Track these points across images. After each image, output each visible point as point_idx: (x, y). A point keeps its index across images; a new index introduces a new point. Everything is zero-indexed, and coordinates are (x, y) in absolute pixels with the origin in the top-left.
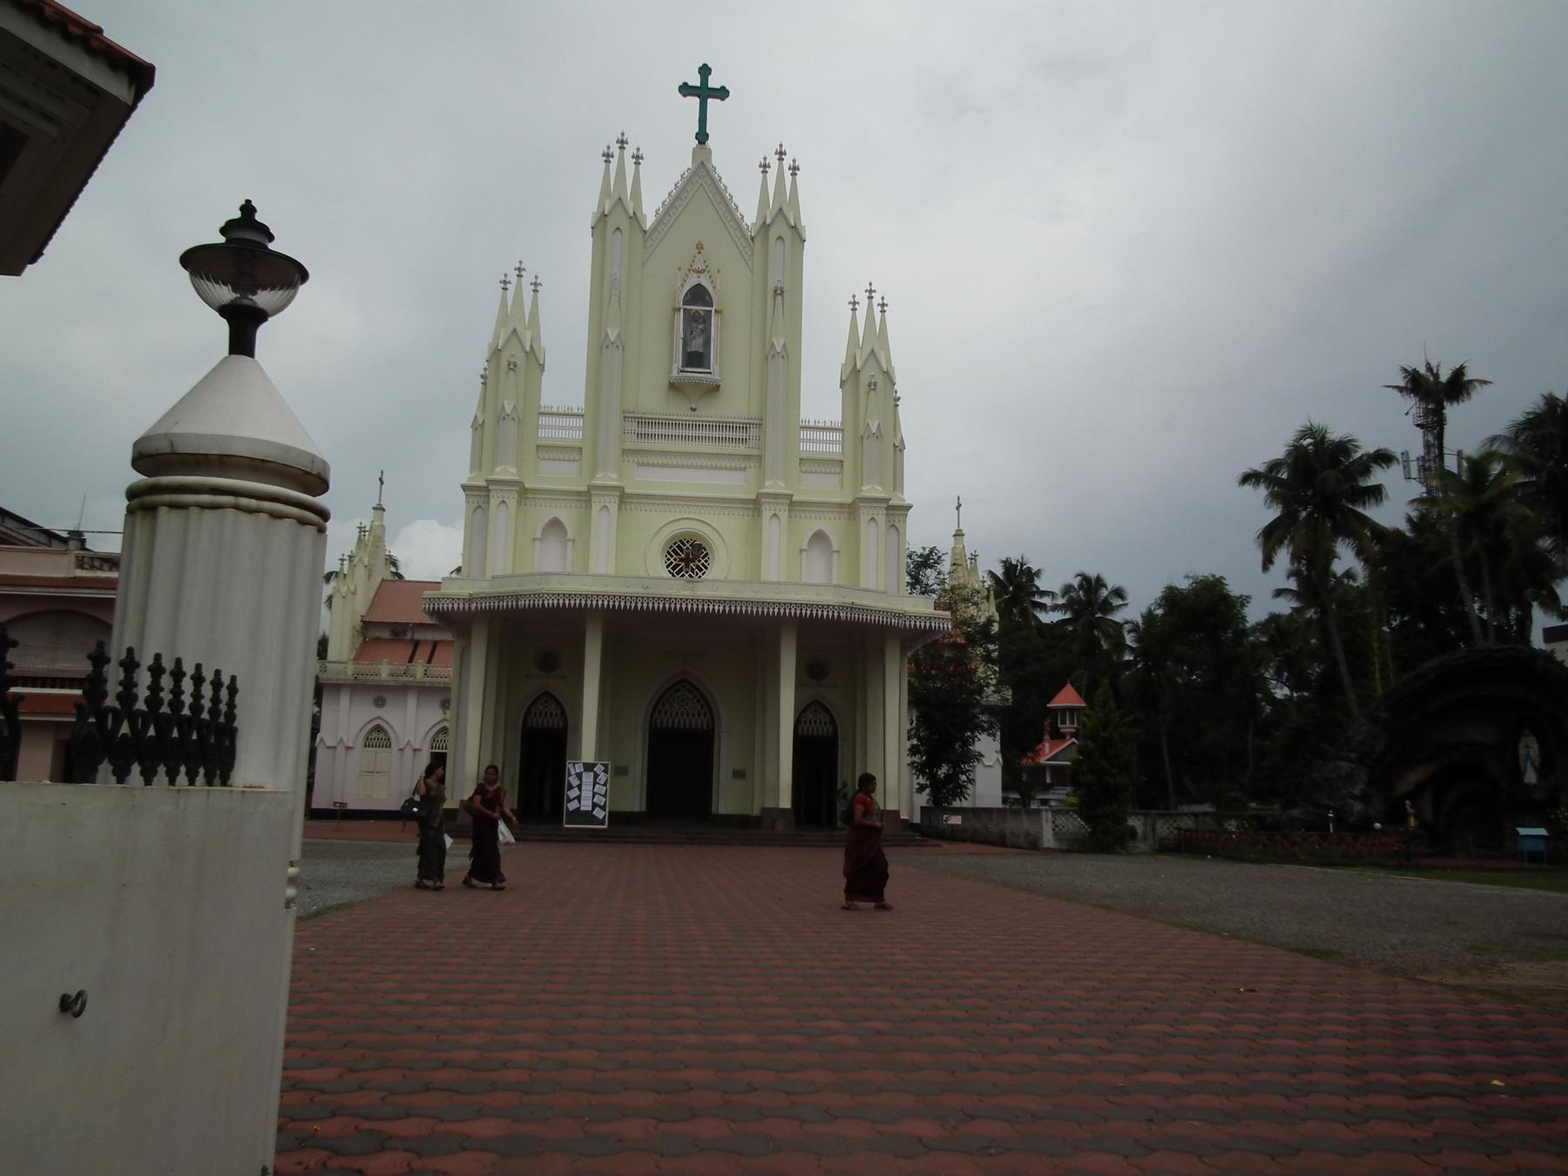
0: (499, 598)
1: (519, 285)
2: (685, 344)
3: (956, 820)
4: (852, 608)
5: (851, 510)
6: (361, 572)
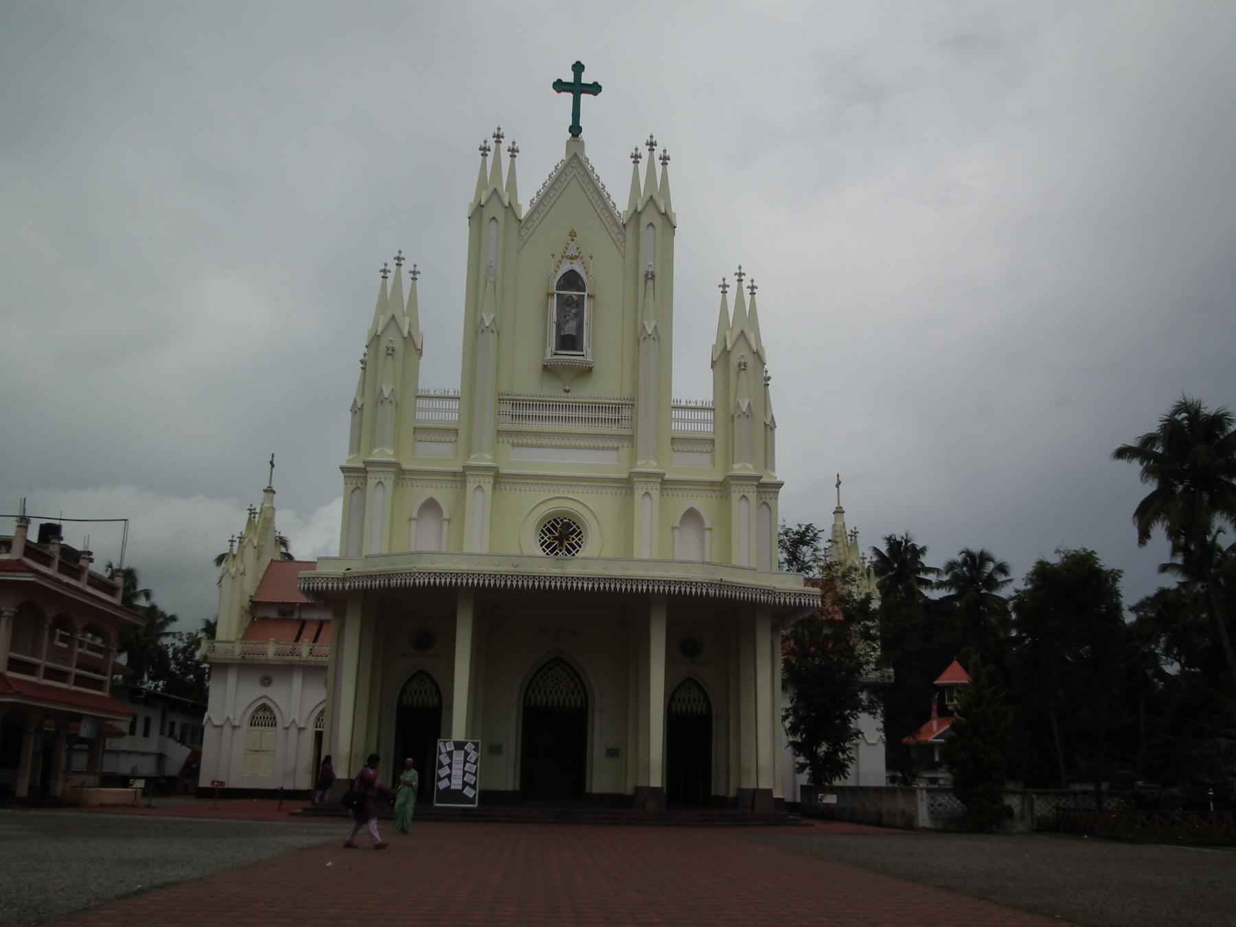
0: (372, 577)
1: (398, 274)
2: (559, 327)
3: (831, 799)
4: (721, 585)
5: (722, 488)
6: (250, 553)
